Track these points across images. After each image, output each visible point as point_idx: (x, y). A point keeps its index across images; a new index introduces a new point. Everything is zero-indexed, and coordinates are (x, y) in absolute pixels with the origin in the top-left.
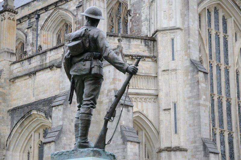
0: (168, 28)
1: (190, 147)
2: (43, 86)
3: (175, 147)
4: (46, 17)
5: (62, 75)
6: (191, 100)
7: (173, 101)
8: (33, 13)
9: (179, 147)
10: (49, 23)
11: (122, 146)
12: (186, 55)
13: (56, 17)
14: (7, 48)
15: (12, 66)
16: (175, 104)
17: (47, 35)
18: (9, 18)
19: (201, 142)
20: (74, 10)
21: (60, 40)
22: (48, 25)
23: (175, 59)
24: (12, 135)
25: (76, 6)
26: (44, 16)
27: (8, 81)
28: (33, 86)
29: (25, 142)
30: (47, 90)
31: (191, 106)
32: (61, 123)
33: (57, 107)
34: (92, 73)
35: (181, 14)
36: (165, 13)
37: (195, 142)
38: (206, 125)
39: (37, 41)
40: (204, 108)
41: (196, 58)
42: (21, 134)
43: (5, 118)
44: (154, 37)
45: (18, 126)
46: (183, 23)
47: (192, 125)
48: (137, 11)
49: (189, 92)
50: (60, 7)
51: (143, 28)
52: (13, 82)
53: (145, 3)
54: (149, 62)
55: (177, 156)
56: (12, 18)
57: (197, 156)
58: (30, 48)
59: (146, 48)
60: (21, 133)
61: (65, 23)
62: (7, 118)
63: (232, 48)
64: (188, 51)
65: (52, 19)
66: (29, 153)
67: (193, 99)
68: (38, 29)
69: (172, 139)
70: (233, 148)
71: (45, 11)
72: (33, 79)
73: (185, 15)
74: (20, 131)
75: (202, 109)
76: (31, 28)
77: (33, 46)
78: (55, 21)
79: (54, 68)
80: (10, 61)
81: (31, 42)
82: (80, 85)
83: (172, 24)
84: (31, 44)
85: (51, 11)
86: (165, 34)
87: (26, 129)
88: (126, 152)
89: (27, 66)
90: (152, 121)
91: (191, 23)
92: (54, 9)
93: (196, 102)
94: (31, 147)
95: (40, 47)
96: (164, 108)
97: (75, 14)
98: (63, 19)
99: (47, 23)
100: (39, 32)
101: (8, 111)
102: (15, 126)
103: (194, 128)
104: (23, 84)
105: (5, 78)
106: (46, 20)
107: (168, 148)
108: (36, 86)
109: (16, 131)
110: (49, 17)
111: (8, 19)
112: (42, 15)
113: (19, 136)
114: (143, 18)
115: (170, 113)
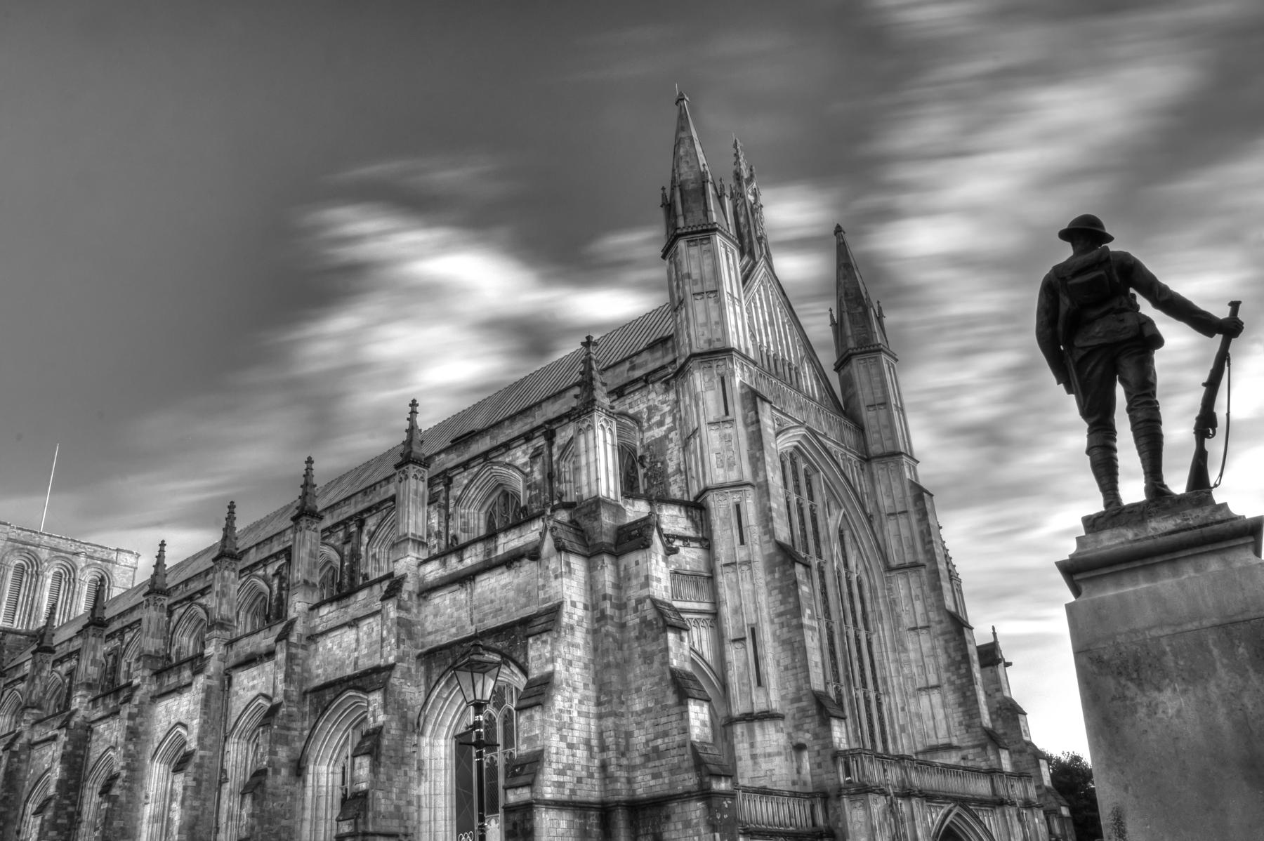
0: (728, 484)
1: (789, 710)
2: (492, 602)
3: (761, 712)
4: (466, 482)
6: (783, 619)
7: (749, 623)
8: (437, 476)
9: (768, 712)
10: (472, 491)
11: (676, 710)
12: (765, 534)
16: (753, 631)
18: (415, 475)
19: (813, 697)
20: (525, 464)
22: (470, 495)
23: (745, 541)
24: (430, 704)
26: (462, 479)
27: (414, 597)
28: (469, 603)
30: (501, 609)
31: (785, 630)
32: (549, 668)
33: (538, 636)
35: (750, 458)
36: (718, 456)
37: (799, 700)
38: (816, 666)
39: (447, 527)
40: (810, 633)
41: (785, 539)
43: (413, 671)
44: (699, 501)
45: (441, 686)
46: (755, 473)
47: (789, 667)
48: (658, 458)
49: (778, 603)
50: (494, 460)
51: (671, 488)
52: (425, 598)
53: (672, 442)
54: (696, 550)
55: (766, 731)
57: (806, 726)
58: (435, 542)
59: (689, 524)
60: (446, 699)
61: (504, 491)
62: (417, 671)
63: (825, 528)
64: (770, 526)
65: (478, 484)
67: (788, 616)
69: (754, 697)
71: (462, 470)
72: (469, 590)
73: (758, 459)
74: (445, 696)
75: (808, 634)
76: (437, 504)
77: (441, 538)
80: (417, 558)
81: (436, 529)
83: (733, 476)
84: (436, 534)
85: (476, 469)
86: (722, 495)
88: (688, 720)
90: (710, 663)
91: (770, 475)
93: (794, 622)
95: (455, 537)
96: (732, 638)
100: (451, 510)
101: (419, 657)
102: (434, 687)
103: (794, 671)
104: (447, 602)
106: (467, 487)
107: (747, 714)
108: (476, 603)
109: (437, 697)
110: (472, 481)
112: (458, 477)
114: (670, 470)
115: (745, 647)
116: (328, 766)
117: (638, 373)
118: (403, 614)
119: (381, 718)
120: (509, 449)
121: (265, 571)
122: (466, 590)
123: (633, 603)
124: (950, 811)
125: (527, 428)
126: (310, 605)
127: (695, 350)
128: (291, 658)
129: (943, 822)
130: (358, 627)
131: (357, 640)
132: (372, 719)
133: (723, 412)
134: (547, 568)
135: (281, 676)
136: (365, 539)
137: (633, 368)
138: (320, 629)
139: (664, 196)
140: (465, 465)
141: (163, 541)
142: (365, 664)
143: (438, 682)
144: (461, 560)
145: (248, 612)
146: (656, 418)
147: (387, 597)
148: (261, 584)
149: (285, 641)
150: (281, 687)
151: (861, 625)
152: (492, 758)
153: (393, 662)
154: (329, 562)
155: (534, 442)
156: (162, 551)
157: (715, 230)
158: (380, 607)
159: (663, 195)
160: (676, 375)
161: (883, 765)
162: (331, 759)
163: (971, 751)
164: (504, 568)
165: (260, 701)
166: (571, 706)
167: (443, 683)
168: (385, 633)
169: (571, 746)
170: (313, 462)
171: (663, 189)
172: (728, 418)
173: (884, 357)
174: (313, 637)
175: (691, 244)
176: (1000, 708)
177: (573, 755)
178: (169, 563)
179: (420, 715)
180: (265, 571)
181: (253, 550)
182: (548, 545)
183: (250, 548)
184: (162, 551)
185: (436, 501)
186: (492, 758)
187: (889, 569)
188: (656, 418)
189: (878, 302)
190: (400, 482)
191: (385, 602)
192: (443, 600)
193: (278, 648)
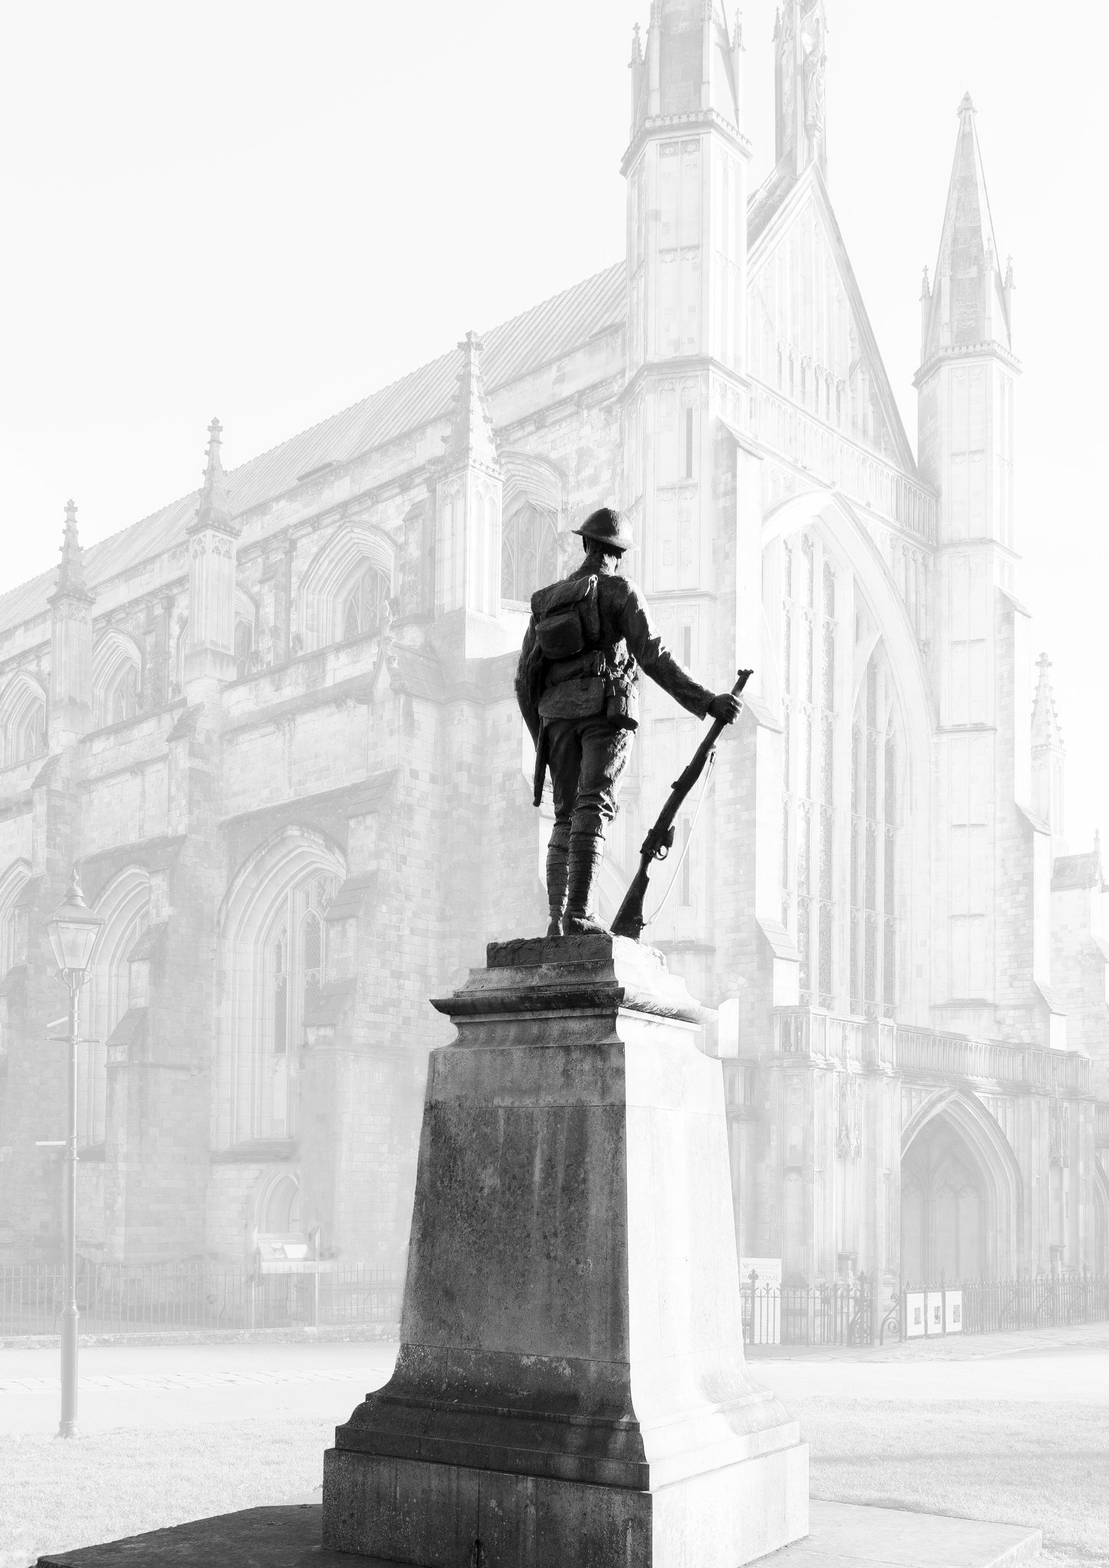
4: (315, 550)
5: (372, 726)
8: (275, 536)
9: (692, 942)
13: (343, 547)
14: (212, 641)
15: (226, 695)
17: (316, 605)
18: (216, 548)
20: (399, 528)
21: (356, 621)
22: (320, 572)
25: (402, 517)
29: (266, 915)
32: (372, 866)
34: (608, 715)
42: (258, 894)
45: (248, 871)
50: (356, 518)
56: (223, 550)
58: (270, 643)
61: (370, 568)
66: (279, 947)
67: (738, 806)
68: (292, 586)
70: (830, 947)
71: (310, 529)
74: (254, 885)
76: (272, 583)
78: (340, 560)
79: (351, 703)
81: (272, 623)
82: (567, 752)
85: (330, 531)
87: (270, 880)
89: (268, 695)
92: (338, 524)
94: (285, 931)
95: (298, 639)
97: (401, 540)
98: (364, 557)
99: (317, 566)
100: (293, 594)
101: (221, 827)
102: (239, 871)
105: (207, 731)
106: (316, 559)
111: (213, 551)
112: (304, 541)
113: (252, 898)
116: (111, 965)
117: (568, 389)
118: (198, 763)
119: (167, 911)
120: (378, 502)
121: (38, 665)
122: (284, 735)
123: (498, 778)
124: (941, 1098)
125: (403, 469)
126: (80, 736)
127: (653, 358)
128: (54, 813)
129: (926, 1112)
130: (143, 775)
131: (143, 794)
132: (154, 911)
133: (684, 474)
134: (381, 717)
135: (42, 837)
136: (175, 629)
137: (561, 379)
138: (93, 773)
139: (636, 42)
140: (314, 522)
141: (215, 421)
142: (154, 830)
143: (244, 864)
144: (278, 689)
145: (20, 725)
146: (588, 472)
147: (175, 736)
148: (34, 685)
149: (44, 788)
150: (43, 853)
151: (880, 815)
152: (314, 975)
153: (184, 833)
154: (127, 659)
155: (413, 493)
156: (71, 521)
157: (710, 124)
158: (166, 750)
159: (634, 40)
160: (621, 399)
161: (844, 1029)
162: (114, 956)
163: (1012, 1013)
164: (333, 708)
165: (21, 869)
166: (402, 920)
167: (250, 868)
168: (173, 789)
169: (398, 975)
170: (221, 429)
171: (637, 28)
172: (690, 481)
173: (996, 364)
174: (85, 785)
175: (667, 151)
176: (1081, 952)
177: (400, 987)
178: (87, 539)
179: (220, 909)
180: (38, 665)
181: (21, 631)
182: (384, 681)
183: (16, 628)
184: (71, 521)
185: (272, 578)
186: (314, 975)
187: (940, 730)
188: (588, 472)
189: (1009, 258)
190: (195, 557)
191: (173, 744)
192: (251, 744)
193: (36, 797)
